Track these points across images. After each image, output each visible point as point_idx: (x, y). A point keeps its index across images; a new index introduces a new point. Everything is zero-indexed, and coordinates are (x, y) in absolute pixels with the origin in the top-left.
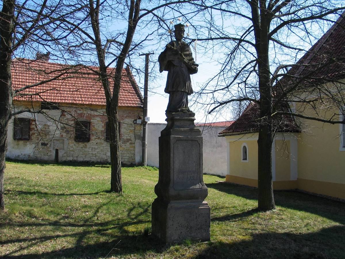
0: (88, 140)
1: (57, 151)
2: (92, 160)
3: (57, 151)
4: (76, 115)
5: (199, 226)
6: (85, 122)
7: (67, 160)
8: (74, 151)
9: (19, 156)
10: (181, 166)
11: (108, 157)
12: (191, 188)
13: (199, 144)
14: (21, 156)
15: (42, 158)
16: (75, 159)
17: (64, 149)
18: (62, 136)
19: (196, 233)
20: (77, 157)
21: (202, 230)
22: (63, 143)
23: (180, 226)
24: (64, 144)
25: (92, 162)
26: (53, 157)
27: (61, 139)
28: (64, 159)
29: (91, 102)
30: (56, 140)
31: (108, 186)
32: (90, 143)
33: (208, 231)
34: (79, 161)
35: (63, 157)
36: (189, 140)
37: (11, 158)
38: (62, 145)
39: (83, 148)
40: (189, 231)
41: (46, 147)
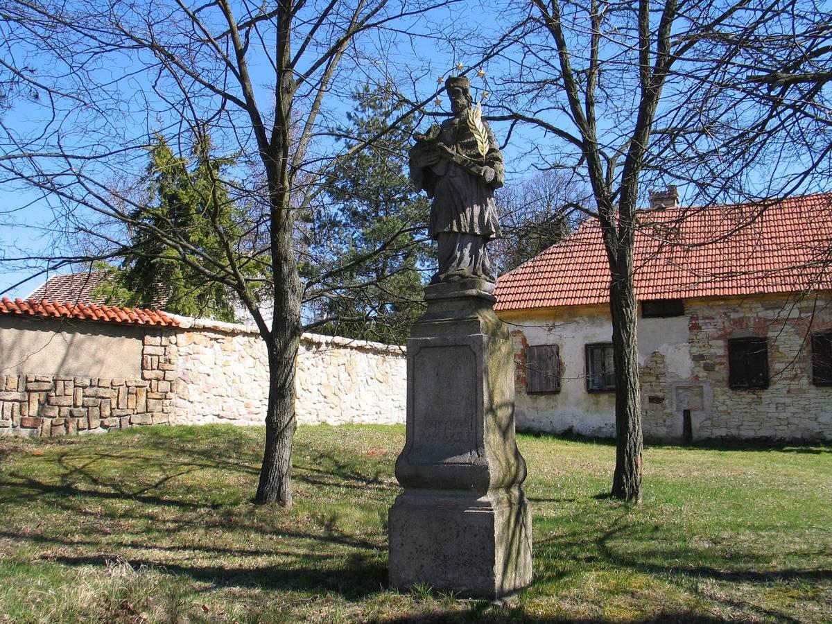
0: (765, 383)
1: (687, 414)
2: (780, 434)
3: (687, 414)
4: (727, 324)
5: (466, 557)
6: (753, 338)
7: (714, 436)
8: (729, 414)
9: (600, 428)
10: (430, 408)
11: (822, 426)
12: (449, 460)
13: (475, 354)
14: (605, 430)
15: (652, 433)
16: (734, 432)
17: (703, 409)
18: (697, 377)
19: (458, 573)
20: (738, 427)
21: (475, 570)
22: (701, 394)
23: (420, 549)
24: (702, 398)
25: (778, 441)
26: (679, 430)
27: (694, 385)
28: (705, 434)
29: (761, 289)
30: (684, 388)
31: (608, 487)
32: (770, 389)
33: (489, 572)
34: (744, 438)
35: (702, 427)
36: (450, 346)
37: (584, 433)
38: (698, 399)
39: (753, 406)
40: (440, 565)
41: (659, 405)
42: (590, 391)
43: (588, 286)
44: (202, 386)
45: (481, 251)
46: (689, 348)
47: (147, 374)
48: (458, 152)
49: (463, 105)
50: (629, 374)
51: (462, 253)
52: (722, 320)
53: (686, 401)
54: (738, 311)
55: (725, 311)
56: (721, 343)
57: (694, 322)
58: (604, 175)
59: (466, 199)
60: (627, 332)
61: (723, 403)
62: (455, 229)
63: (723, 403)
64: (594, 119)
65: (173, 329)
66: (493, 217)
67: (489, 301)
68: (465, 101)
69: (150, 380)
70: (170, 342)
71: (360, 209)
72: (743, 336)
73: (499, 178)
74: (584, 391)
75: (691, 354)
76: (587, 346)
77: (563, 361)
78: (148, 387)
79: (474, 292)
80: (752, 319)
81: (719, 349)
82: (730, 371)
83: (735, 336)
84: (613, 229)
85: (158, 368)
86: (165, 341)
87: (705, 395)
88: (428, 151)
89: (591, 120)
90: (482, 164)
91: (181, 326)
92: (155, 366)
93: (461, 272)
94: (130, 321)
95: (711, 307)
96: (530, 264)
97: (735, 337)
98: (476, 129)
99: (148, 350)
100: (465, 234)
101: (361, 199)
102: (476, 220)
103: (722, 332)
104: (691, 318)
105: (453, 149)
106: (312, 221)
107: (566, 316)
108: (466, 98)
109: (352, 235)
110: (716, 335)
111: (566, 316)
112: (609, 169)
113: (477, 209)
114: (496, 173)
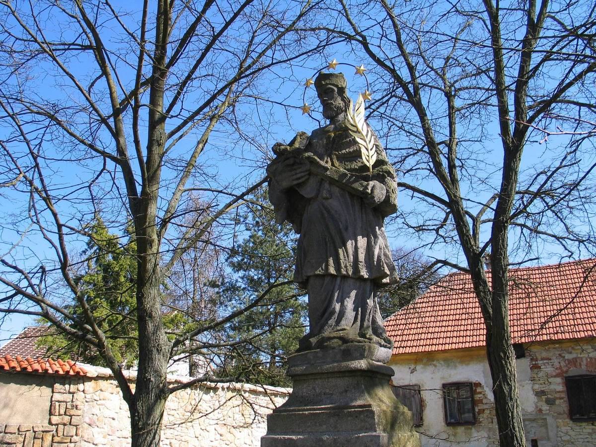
4: (563, 364)
17: (549, 439)
18: (540, 410)
22: (545, 425)
24: (547, 428)
29: (590, 333)
38: (543, 430)
42: (448, 424)
43: (442, 335)
44: (107, 429)
45: (370, 302)
46: (531, 385)
47: (55, 419)
48: (333, 165)
49: (339, 108)
50: (514, 429)
51: (342, 305)
52: (558, 360)
53: (533, 431)
54: (571, 353)
55: (559, 352)
56: (559, 380)
57: (534, 363)
58: (471, 233)
59: (346, 229)
60: (508, 384)
61: (567, 433)
62: (332, 270)
63: (567, 433)
64: (457, 181)
65: (81, 378)
66: (385, 255)
67: (384, 374)
68: (341, 102)
69: (57, 425)
70: (78, 390)
71: (256, 277)
72: (577, 374)
73: (392, 199)
74: (443, 424)
75: (533, 390)
76: (444, 386)
77: (424, 398)
78: (54, 432)
79: (362, 364)
80: (584, 359)
81: (558, 385)
82: (570, 405)
83: (570, 374)
84: (485, 282)
85: (65, 414)
86: (73, 388)
87: (549, 427)
88: (293, 165)
89: (454, 181)
90: (367, 179)
91: (88, 375)
92: (62, 412)
93: (341, 333)
94: (40, 371)
95: (548, 350)
96: (393, 317)
97: (571, 375)
98: (358, 132)
99: (57, 397)
100: (345, 277)
101: (256, 268)
102: (362, 256)
103: (559, 371)
104: (531, 359)
105: (327, 162)
106: (218, 286)
107: (425, 361)
108: (343, 100)
109: (250, 297)
110: (554, 374)
111: (425, 361)
112: (474, 225)
113: (362, 242)
114: (387, 191)
